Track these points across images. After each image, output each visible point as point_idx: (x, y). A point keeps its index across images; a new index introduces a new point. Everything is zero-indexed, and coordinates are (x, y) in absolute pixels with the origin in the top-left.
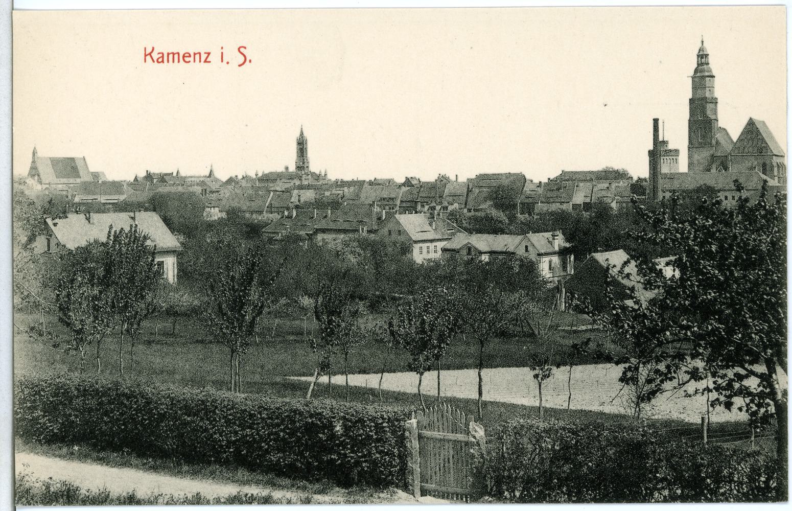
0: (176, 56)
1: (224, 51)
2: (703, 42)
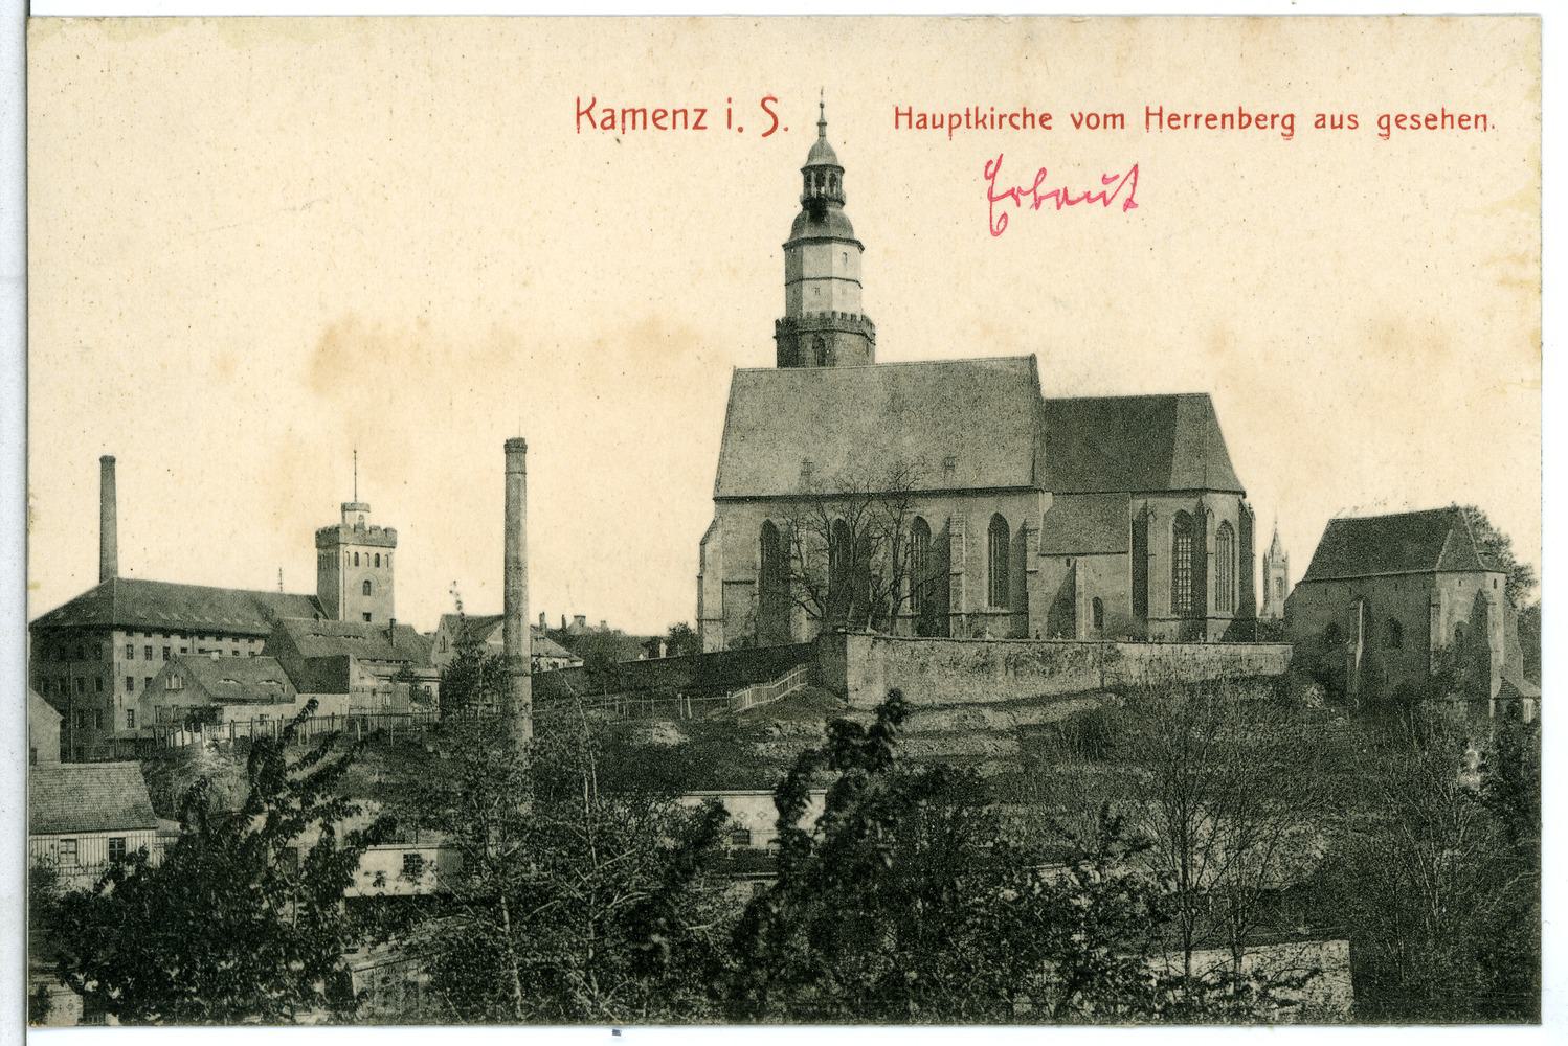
0: (640, 116)
1: (733, 106)
2: (822, 124)
